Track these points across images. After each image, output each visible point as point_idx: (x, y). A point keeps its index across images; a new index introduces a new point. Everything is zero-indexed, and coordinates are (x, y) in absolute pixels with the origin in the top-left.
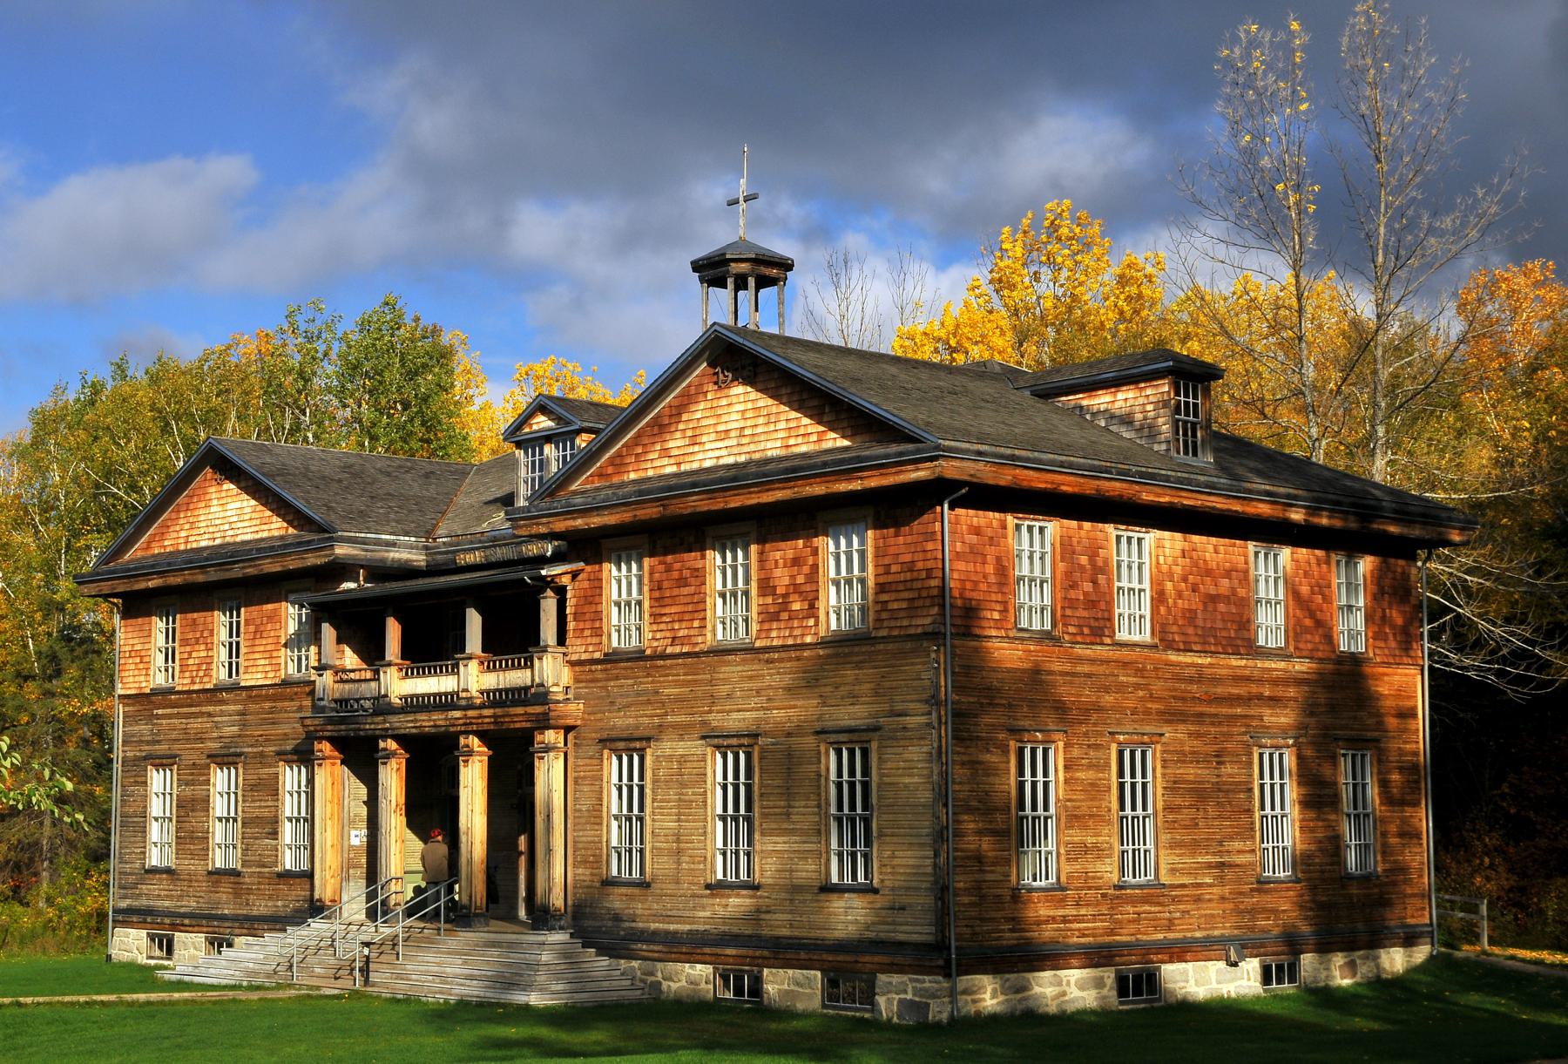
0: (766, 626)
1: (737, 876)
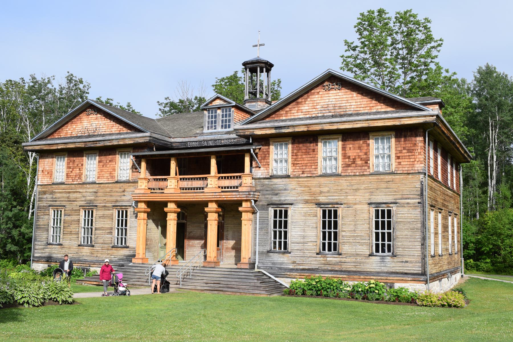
0: (345, 168)
1: (122, 244)
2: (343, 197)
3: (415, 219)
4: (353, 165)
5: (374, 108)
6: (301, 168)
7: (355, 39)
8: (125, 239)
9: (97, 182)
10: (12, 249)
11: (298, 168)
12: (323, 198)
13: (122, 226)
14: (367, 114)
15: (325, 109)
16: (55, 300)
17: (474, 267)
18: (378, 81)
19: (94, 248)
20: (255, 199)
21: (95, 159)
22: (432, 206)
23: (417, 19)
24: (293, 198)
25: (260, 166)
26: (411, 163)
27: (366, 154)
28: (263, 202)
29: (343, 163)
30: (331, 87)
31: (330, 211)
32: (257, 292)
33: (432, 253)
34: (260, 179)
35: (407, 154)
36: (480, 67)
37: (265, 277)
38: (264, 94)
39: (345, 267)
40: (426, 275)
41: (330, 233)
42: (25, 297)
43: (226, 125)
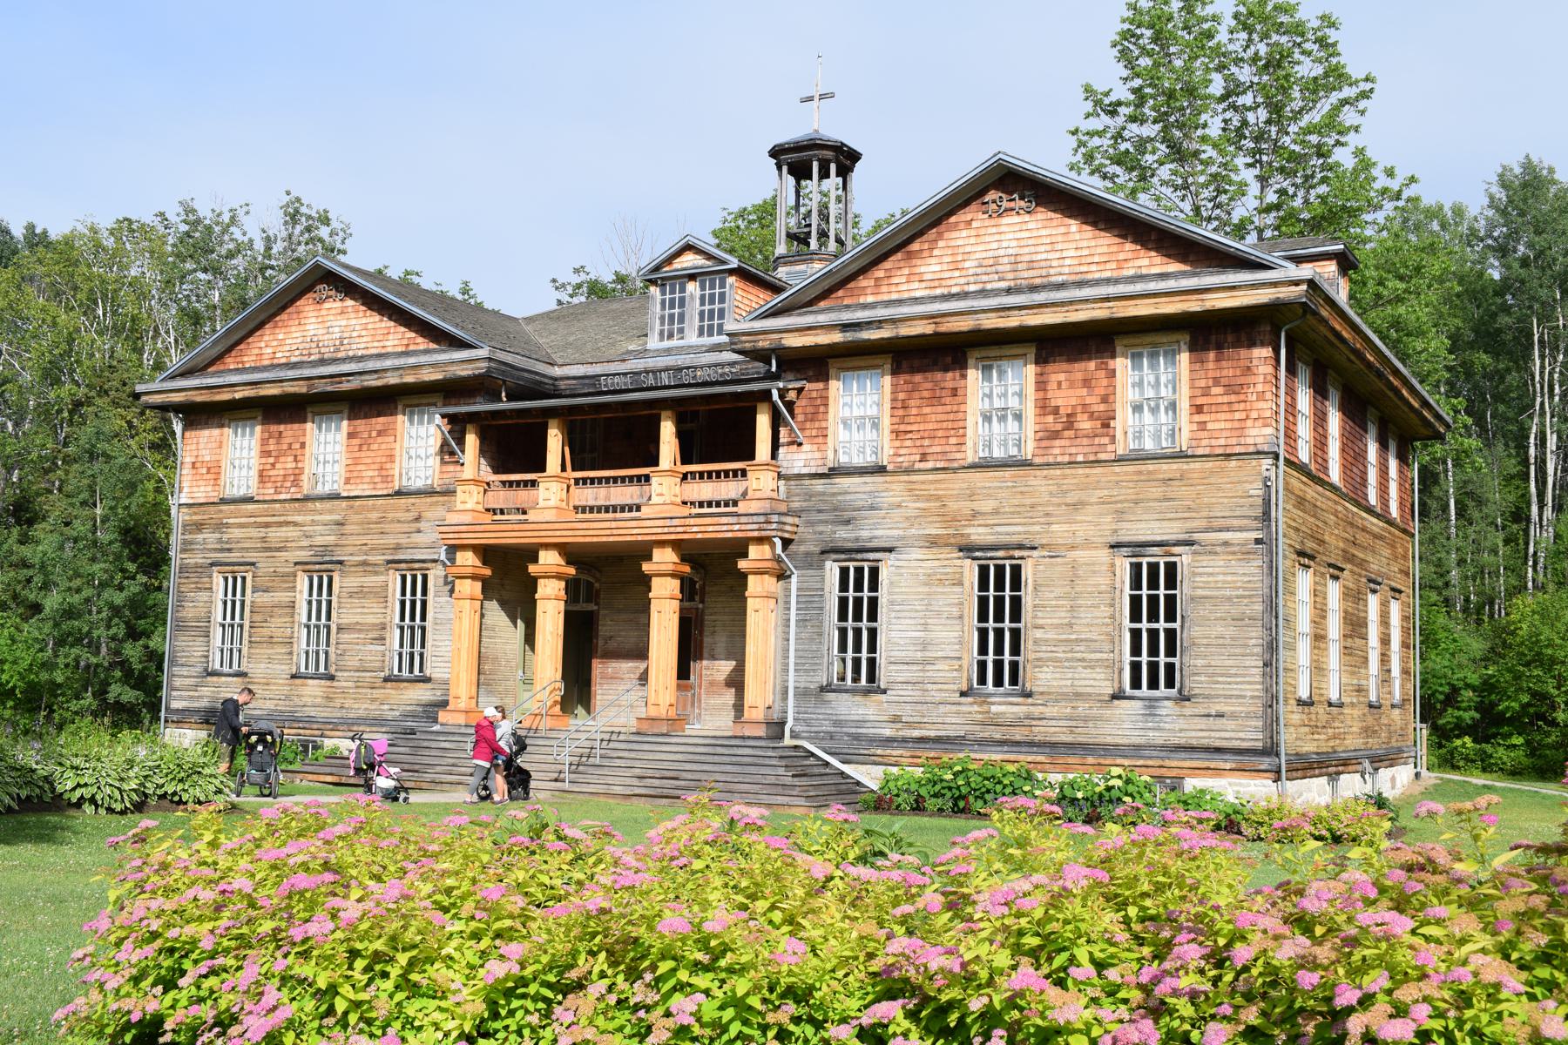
1: (411, 671)
2: (1037, 528)
3: (1245, 589)
4: (1067, 433)
5: (1131, 264)
6: (918, 443)
7: (1114, 81)
8: (422, 655)
9: (344, 494)
10: (124, 699)
11: (908, 443)
12: (981, 530)
13: (413, 618)
14: (1108, 281)
15: (989, 270)
16: (176, 799)
17: (1473, 761)
18: (1181, 205)
19: (335, 684)
20: (786, 535)
21: (338, 429)
22: (1301, 554)
23: (1297, 16)
24: (895, 533)
25: (801, 439)
26: (1236, 425)
27: (1105, 399)
28: (808, 544)
29: (1037, 428)
30: (1005, 204)
31: (1000, 570)
32: (780, 800)
33: (1304, 693)
34: (800, 477)
35: (1225, 399)
36: (1504, 167)
37: (812, 761)
38: (832, 238)
39: (1041, 732)
40: (1278, 755)
41: (999, 633)
42: (86, 785)
43: (711, 327)
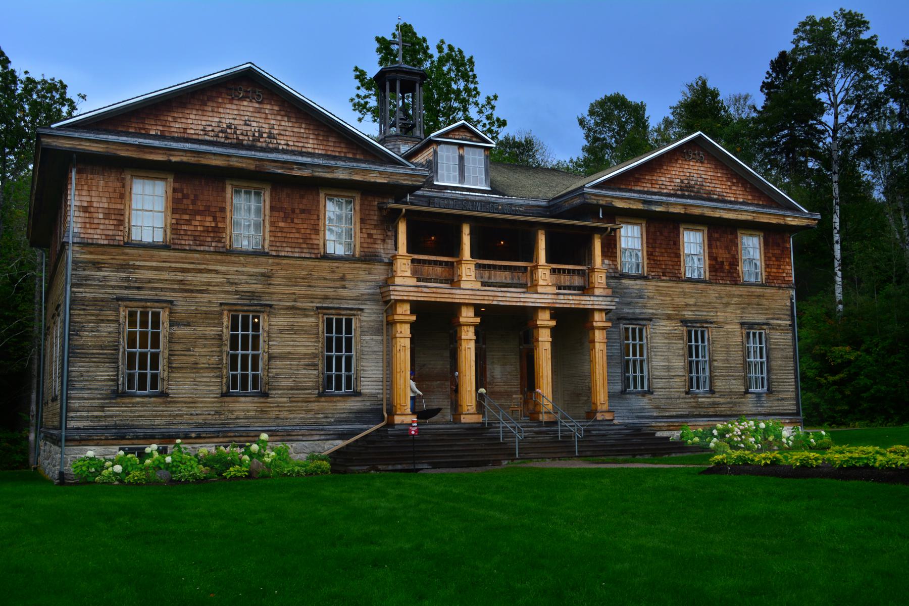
2: (712, 314)
12: (690, 313)
19: (269, 400)
